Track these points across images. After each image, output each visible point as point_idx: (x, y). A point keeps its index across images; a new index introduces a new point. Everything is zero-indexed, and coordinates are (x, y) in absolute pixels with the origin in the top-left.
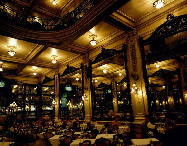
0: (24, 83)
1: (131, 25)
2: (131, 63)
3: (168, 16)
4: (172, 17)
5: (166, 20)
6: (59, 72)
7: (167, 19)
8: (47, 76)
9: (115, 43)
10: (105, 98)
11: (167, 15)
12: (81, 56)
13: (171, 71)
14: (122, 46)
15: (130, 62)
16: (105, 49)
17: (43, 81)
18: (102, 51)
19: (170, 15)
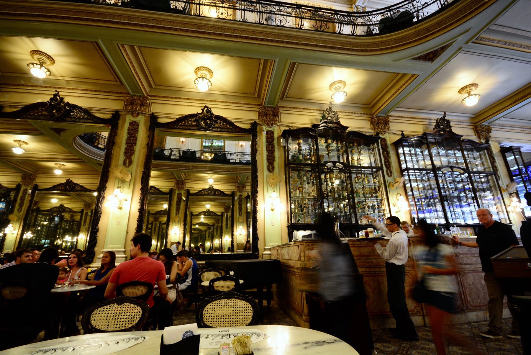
2: (123, 150)
3: (205, 107)
4: (209, 111)
5: (200, 111)
7: (203, 110)
9: (363, 121)
10: (144, 234)
11: (204, 105)
12: (280, 107)
14: (112, 114)
15: (120, 147)
16: (62, 99)
18: (51, 99)
19: (208, 107)
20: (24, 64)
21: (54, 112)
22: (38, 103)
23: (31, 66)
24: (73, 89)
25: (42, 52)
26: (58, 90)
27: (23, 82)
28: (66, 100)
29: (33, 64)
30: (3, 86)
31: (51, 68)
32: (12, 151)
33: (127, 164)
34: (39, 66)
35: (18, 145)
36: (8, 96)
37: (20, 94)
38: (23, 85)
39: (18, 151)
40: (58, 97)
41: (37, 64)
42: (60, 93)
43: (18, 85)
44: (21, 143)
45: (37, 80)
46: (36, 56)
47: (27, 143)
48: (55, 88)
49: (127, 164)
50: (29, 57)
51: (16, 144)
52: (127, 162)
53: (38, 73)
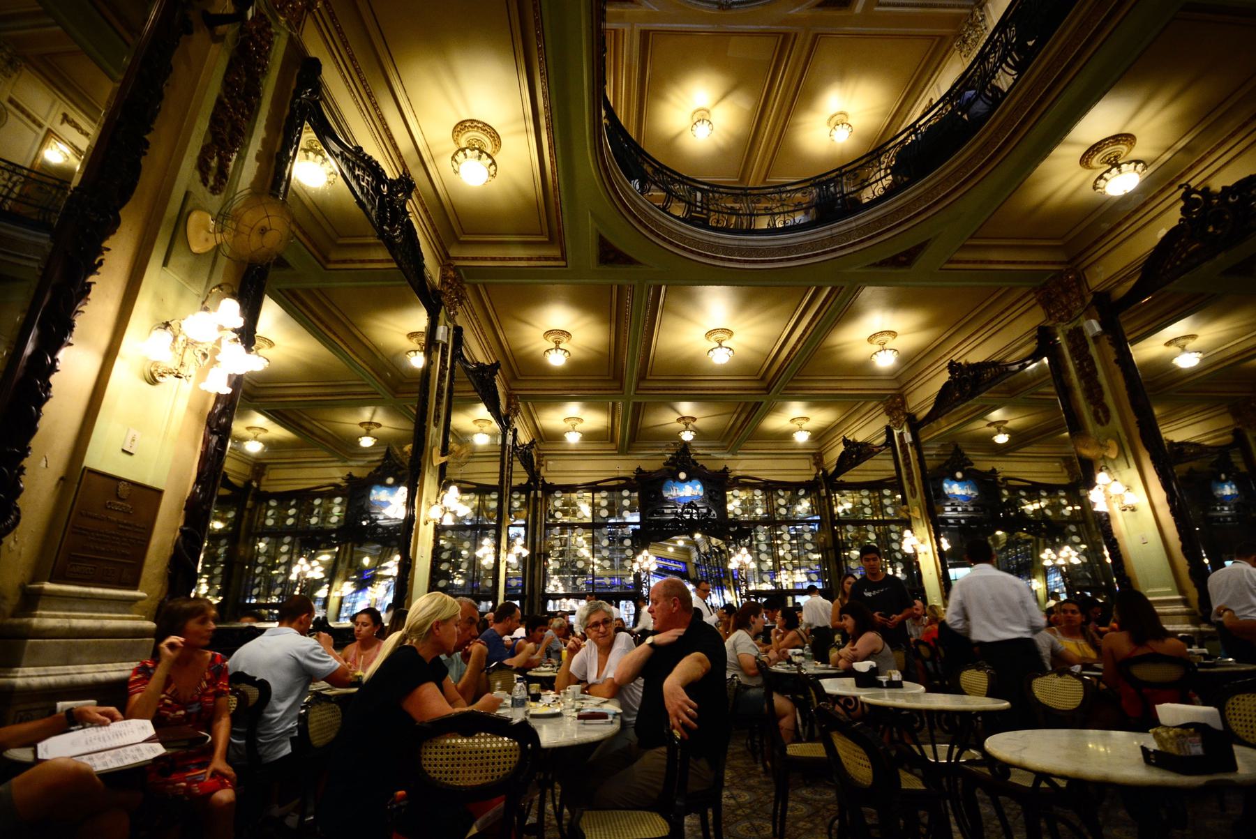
0: (765, 478)
1: (1045, 263)
6: (911, 405)
8: (851, 439)
9: (1028, 314)
13: (1208, 447)
16: (1206, 192)
17: (838, 464)
18: (1183, 210)
20: (1088, 191)
21: (1211, 229)
22: (1164, 238)
23: (1101, 183)
24: (1210, 153)
25: (1100, 143)
26: (1184, 181)
27: (1106, 226)
28: (1216, 185)
29: (1101, 177)
30: (1081, 259)
31: (1137, 153)
32: (1175, 366)
33: (1103, 419)
34: (1115, 170)
35: (1178, 349)
36: (1101, 268)
37: (1117, 251)
38: (1112, 230)
39: (1187, 361)
40: (1194, 196)
41: (1108, 171)
42: (1193, 184)
43: (1103, 237)
44: (1181, 342)
45: (1126, 199)
46: (1095, 161)
47: (1193, 337)
48: (1171, 184)
49: (1103, 419)
50: (1086, 173)
51: (1173, 349)
52: (1101, 414)
53: (1122, 183)
